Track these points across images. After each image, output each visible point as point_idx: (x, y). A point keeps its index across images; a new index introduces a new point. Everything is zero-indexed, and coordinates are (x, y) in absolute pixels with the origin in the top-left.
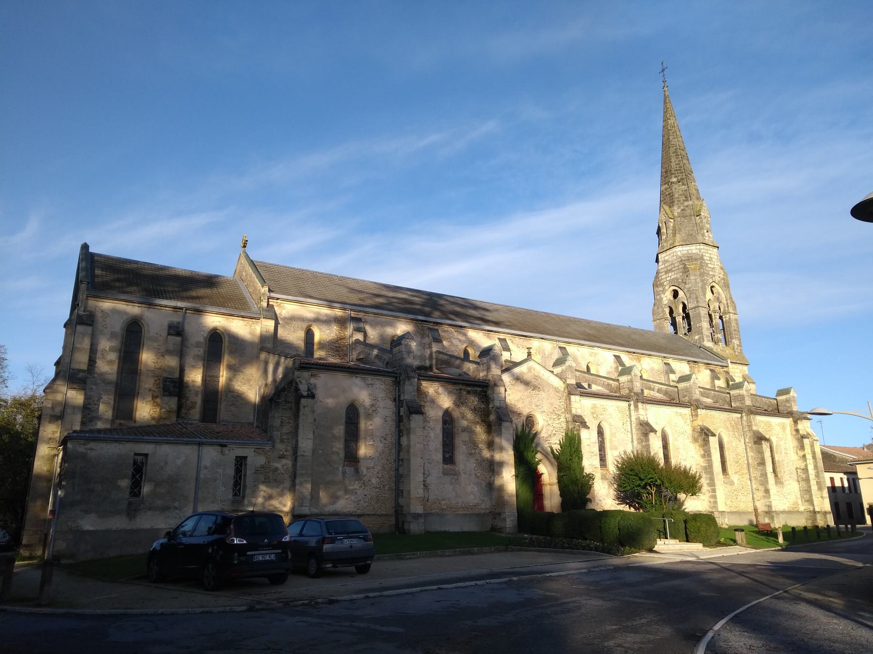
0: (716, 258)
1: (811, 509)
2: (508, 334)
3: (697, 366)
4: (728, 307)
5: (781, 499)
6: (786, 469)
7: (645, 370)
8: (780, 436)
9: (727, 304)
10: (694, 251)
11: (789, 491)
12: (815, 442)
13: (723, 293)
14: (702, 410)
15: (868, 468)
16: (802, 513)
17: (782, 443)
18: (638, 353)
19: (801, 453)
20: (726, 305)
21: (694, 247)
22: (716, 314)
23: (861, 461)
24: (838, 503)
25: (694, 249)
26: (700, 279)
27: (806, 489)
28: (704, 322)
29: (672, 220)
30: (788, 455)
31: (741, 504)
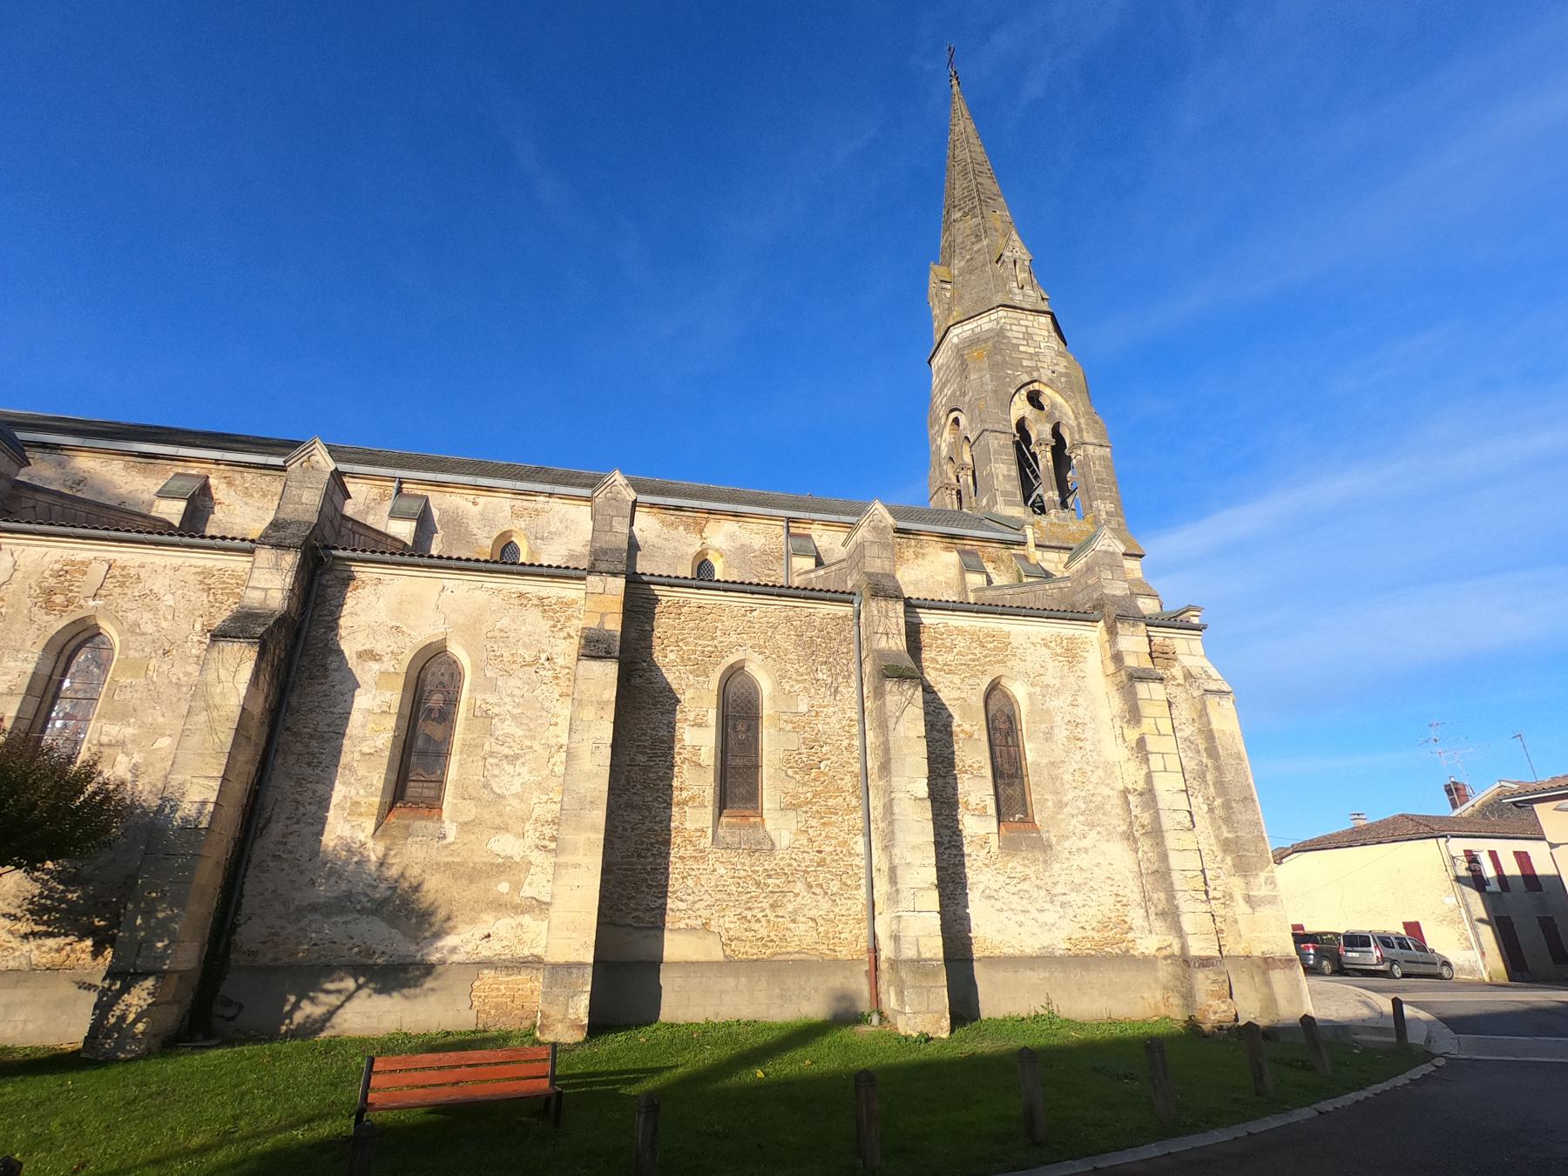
0: (1046, 334)
1: (1176, 949)
2: (217, 462)
3: (913, 542)
4: (1080, 431)
5: (1034, 913)
6: (1071, 795)
7: (717, 550)
8: (1049, 680)
9: (1079, 425)
10: (985, 327)
11: (1078, 878)
12: (1212, 701)
13: (1065, 404)
14: (610, 579)
15: (1555, 809)
16: (1147, 962)
17: (1058, 703)
18: (693, 510)
19: (1132, 735)
20: (1076, 429)
21: (987, 319)
22: (1043, 447)
23: (1544, 790)
24: (1551, 918)
25: (985, 323)
26: (992, 376)
27: (1155, 867)
28: (996, 461)
29: (948, 286)
30: (1088, 746)
31: (802, 928)
